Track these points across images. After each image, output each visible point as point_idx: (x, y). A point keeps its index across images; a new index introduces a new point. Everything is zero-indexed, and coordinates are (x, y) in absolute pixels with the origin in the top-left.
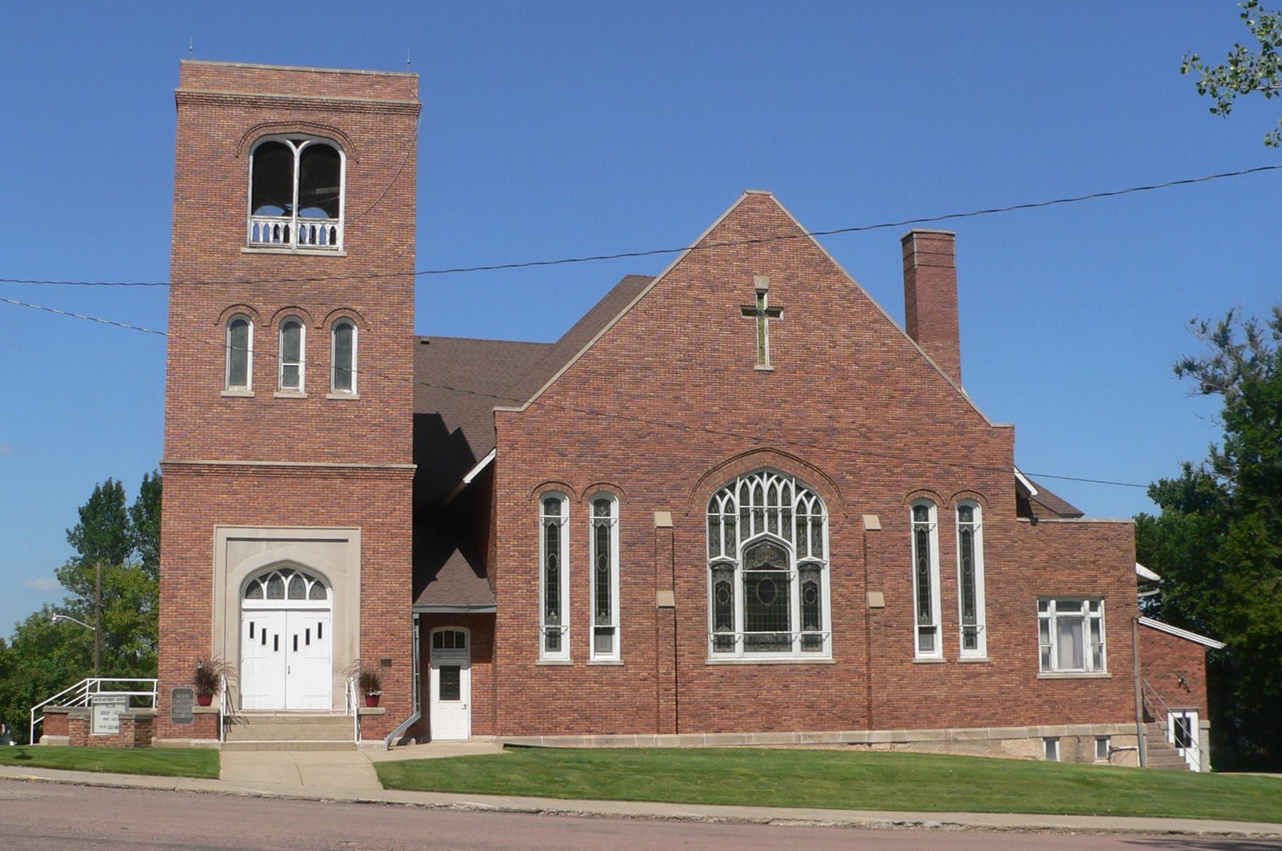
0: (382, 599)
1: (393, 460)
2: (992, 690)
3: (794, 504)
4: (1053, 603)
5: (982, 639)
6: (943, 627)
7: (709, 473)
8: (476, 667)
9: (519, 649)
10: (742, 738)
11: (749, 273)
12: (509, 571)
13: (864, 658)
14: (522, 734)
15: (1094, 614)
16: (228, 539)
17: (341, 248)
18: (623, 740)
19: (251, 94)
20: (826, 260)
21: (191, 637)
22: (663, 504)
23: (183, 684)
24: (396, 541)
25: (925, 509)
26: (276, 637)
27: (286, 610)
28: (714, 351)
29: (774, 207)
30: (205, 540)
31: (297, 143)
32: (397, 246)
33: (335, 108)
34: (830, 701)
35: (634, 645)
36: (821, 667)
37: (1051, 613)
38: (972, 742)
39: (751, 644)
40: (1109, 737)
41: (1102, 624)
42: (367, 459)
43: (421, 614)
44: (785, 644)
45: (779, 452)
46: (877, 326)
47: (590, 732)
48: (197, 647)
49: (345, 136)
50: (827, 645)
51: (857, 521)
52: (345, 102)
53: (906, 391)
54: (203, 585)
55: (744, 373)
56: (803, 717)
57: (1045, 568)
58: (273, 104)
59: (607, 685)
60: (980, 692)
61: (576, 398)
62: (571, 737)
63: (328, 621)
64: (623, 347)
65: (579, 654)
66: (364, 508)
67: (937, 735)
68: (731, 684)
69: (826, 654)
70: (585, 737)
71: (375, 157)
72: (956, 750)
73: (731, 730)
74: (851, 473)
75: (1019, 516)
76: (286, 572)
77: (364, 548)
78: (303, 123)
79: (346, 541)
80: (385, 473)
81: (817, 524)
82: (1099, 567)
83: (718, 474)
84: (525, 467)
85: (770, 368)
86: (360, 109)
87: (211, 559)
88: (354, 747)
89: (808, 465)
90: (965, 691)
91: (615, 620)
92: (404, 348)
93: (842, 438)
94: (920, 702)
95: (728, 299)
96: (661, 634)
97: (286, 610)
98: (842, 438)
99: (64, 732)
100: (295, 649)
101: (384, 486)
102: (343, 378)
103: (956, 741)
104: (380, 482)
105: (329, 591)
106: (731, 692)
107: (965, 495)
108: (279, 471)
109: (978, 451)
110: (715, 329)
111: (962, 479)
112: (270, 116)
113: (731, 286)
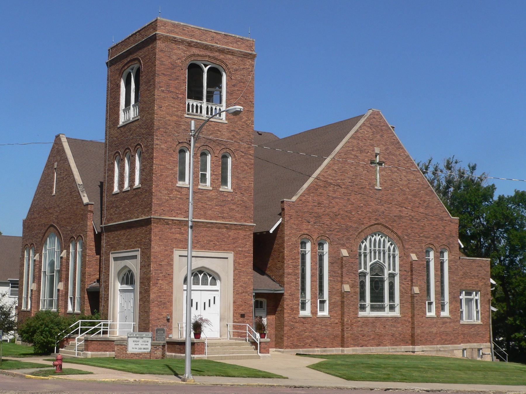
0: (241, 286)
1: (245, 221)
2: (451, 329)
3: (386, 249)
4: (464, 292)
5: (447, 307)
6: (330, 300)
7: (359, 233)
8: (269, 317)
9: (292, 309)
10: (370, 349)
11: (373, 146)
13: (410, 315)
14: (294, 348)
15: (477, 298)
16: (180, 256)
18: (330, 351)
19: (189, 39)
20: (399, 142)
21: (164, 304)
22: (343, 246)
23: (160, 326)
24: (247, 259)
25: (305, 243)
26: (197, 303)
27: (201, 290)
28: (361, 179)
29: (381, 118)
31: (206, 66)
32: (247, 120)
33: (222, 51)
34: (399, 333)
35: (333, 308)
36: (395, 319)
37: (463, 296)
38: (445, 351)
39: (373, 308)
40: (481, 349)
41: (479, 302)
43: (256, 293)
44: (382, 308)
45: (383, 225)
46: (415, 173)
47: (317, 347)
48: (167, 308)
49: (227, 65)
50: (397, 309)
51: (408, 256)
52: (227, 49)
53: (424, 201)
54: (169, 277)
55: (371, 190)
56: (390, 340)
57: (462, 278)
58: (197, 46)
59: (324, 326)
60: (447, 330)
61: (313, 197)
62: (311, 349)
63: (217, 295)
64: (330, 175)
65: (314, 313)
66: (234, 243)
67: (434, 348)
69: (397, 313)
70: (316, 349)
71: (238, 77)
72: (440, 354)
73: (366, 346)
74: (407, 236)
76: (201, 272)
77: (235, 262)
78: (209, 57)
79: (227, 258)
80: (243, 227)
81: (394, 257)
82: (479, 278)
83: (362, 233)
84: (295, 227)
85: (380, 188)
86: (232, 53)
87: (172, 265)
88: (259, 357)
90: (442, 329)
91: (326, 296)
92: (250, 169)
93: (403, 220)
94: (427, 334)
95: (366, 156)
96: (341, 303)
97: (201, 290)
98: (403, 220)
100: (205, 309)
101: (242, 233)
102: (224, 182)
103: (440, 351)
104: (241, 231)
105: (218, 282)
106: (366, 329)
107: (443, 247)
108: (199, 224)
109: (447, 228)
110: (361, 170)
111: (442, 240)
112: (195, 51)
113: (367, 151)
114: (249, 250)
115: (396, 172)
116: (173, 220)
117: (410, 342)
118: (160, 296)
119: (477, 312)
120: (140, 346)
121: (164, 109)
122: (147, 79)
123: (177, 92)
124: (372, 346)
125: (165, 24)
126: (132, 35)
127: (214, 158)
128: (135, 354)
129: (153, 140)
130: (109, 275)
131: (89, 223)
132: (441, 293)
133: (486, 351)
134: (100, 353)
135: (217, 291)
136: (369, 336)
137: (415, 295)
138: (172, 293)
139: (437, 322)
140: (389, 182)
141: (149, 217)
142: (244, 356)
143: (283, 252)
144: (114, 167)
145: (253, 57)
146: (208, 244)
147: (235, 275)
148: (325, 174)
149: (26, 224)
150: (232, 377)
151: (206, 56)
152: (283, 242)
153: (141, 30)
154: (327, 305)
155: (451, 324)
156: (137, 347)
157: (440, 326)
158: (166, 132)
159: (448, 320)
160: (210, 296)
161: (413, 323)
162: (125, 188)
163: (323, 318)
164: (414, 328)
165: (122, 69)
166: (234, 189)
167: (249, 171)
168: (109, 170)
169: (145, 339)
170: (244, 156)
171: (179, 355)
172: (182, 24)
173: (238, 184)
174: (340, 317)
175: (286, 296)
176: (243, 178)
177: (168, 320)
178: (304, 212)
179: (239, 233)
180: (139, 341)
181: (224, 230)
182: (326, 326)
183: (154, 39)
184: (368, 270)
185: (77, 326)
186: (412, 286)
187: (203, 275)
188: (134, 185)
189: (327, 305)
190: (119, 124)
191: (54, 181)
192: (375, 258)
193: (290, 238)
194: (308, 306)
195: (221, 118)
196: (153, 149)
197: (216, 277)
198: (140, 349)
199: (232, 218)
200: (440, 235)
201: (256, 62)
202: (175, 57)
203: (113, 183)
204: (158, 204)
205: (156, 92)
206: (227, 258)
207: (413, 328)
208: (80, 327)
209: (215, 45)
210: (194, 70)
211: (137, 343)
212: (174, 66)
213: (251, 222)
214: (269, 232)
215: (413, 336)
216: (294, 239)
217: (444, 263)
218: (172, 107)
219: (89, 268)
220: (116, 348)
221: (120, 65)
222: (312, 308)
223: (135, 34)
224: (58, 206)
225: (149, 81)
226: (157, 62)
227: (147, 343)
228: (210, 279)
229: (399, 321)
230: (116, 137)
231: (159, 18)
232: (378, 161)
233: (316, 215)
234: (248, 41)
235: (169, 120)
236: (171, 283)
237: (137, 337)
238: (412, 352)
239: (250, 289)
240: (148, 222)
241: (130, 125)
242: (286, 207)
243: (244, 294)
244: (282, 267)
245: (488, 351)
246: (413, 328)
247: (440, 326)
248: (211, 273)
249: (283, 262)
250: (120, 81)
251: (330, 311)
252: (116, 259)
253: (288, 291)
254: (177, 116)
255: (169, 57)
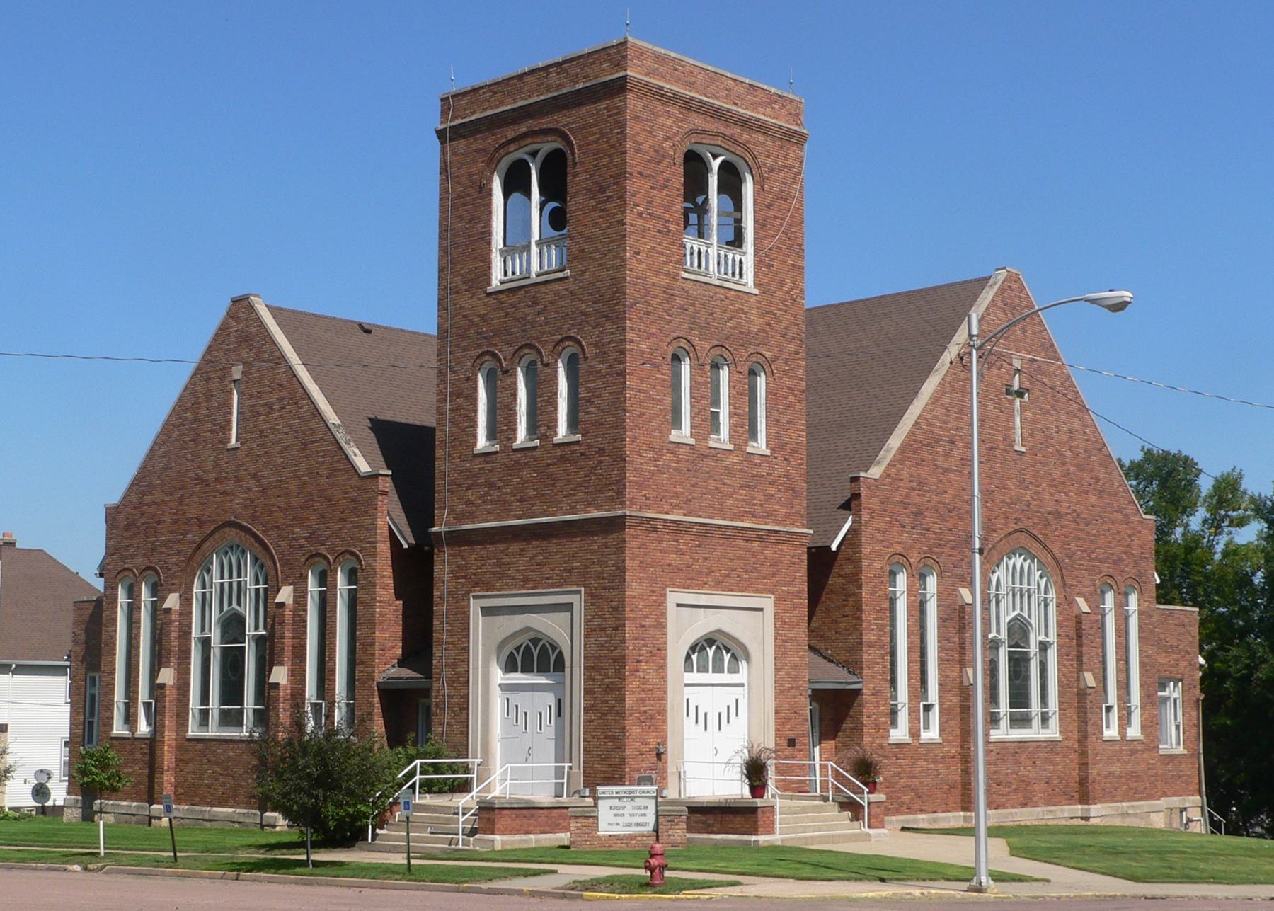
0: (788, 674)
3: (1033, 586)
6: (941, 705)
9: (877, 726)
12: (871, 645)
15: (1175, 695)
16: (678, 605)
17: (751, 283)
18: (944, 819)
20: (1052, 346)
28: (992, 428)
29: (1022, 288)
30: (660, 604)
31: (715, 157)
33: (745, 123)
36: (1052, 743)
38: (1135, 815)
40: (1185, 809)
41: (1179, 703)
42: (777, 522)
45: (1029, 533)
47: (922, 811)
49: (755, 158)
51: (1072, 603)
53: (1097, 479)
54: (658, 654)
60: (1138, 768)
62: (911, 817)
64: (936, 418)
65: (915, 734)
68: (1004, 761)
69: (1053, 732)
70: (921, 816)
72: (1128, 822)
75: (1159, 603)
83: (994, 552)
85: (1023, 449)
86: (763, 128)
87: (665, 627)
89: (1045, 547)
91: (933, 695)
92: (800, 402)
94: (1106, 777)
95: (998, 376)
99: (566, 829)
101: (788, 551)
105: (743, 666)
112: (697, 121)
114: (799, 592)
115: (1048, 412)
116: (665, 521)
117: (1077, 796)
118: (643, 700)
119: (1177, 727)
120: (627, 819)
121: (643, 256)
122: (596, 183)
123: (667, 217)
124: (1013, 807)
125: (641, 53)
126: (532, 72)
127: (737, 377)
128: (618, 838)
129: (623, 330)
130: (467, 649)
131: (380, 522)
132: (1124, 686)
133: (1182, 812)
134: (517, 837)
135: (742, 685)
136: (1008, 785)
137: (1089, 691)
138: (665, 693)
139: (1121, 751)
140: (1038, 436)
141: (619, 513)
142: (839, 835)
143: (858, 596)
144: (476, 389)
145: (798, 139)
146: (728, 576)
147: (777, 648)
148: (929, 417)
149: (120, 517)
150: (1014, 880)
151: (717, 134)
152: (858, 571)
153: (564, 62)
154: (935, 715)
155: (1145, 755)
156: (619, 820)
157: (1126, 759)
158: (647, 313)
159: (1140, 747)
160: (725, 697)
161: (1083, 754)
162: (518, 442)
163: (930, 745)
164: (1087, 764)
165: (497, 150)
166: (772, 449)
167: (798, 407)
168: (455, 395)
169: (638, 802)
170: (788, 371)
171: (705, 836)
172: (672, 54)
173: (778, 438)
174: (957, 743)
175: (867, 696)
176: (789, 423)
177: (659, 756)
178: (894, 504)
179: (782, 550)
180: (624, 808)
181: (756, 544)
182: (935, 762)
183: (620, 86)
184: (1004, 636)
185: (412, 774)
186: (1080, 669)
187: (716, 649)
188: (556, 434)
189: (935, 715)
190: (490, 284)
191: (230, 413)
192: (230, 603)
193: (871, 563)
194: (903, 717)
195: (744, 280)
196: (623, 352)
197: (739, 653)
198: (629, 825)
199: (769, 515)
200: (1124, 557)
201: (806, 153)
202: (660, 134)
203: (474, 425)
204: (636, 483)
205: (629, 218)
206: (761, 610)
207: (1083, 765)
208: (418, 777)
209: (734, 108)
210: (694, 165)
211: (621, 812)
212: (659, 156)
213: (803, 526)
214: (829, 547)
215: (1083, 782)
216: (877, 565)
217: (1126, 618)
218: (658, 252)
219: (382, 631)
220: (573, 825)
221: (490, 142)
222: (910, 723)
223: (546, 69)
224: (254, 475)
225: (603, 189)
226: (629, 145)
227: (643, 812)
228: (727, 657)
229: (1058, 748)
230: (483, 317)
231: (630, 39)
232: (1016, 387)
233: (914, 510)
234: (792, 101)
235: (653, 284)
236: (662, 668)
237: (620, 798)
238: (1082, 818)
239: (803, 682)
240: (616, 524)
241: (534, 289)
242: (864, 492)
243: (793, 692)
244: (856, 630)
245: (1196, 814)
246: (1083, 765)
247: (1126, 759)
248: (729, 644)
249: (859, 618)
250: (490, 181)
251: (942, 730)
252: (487, 611)
253: (868, 685)
254: (667, 274)
255: (651, 133)
